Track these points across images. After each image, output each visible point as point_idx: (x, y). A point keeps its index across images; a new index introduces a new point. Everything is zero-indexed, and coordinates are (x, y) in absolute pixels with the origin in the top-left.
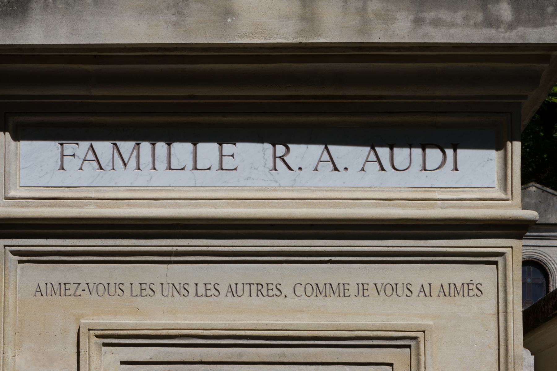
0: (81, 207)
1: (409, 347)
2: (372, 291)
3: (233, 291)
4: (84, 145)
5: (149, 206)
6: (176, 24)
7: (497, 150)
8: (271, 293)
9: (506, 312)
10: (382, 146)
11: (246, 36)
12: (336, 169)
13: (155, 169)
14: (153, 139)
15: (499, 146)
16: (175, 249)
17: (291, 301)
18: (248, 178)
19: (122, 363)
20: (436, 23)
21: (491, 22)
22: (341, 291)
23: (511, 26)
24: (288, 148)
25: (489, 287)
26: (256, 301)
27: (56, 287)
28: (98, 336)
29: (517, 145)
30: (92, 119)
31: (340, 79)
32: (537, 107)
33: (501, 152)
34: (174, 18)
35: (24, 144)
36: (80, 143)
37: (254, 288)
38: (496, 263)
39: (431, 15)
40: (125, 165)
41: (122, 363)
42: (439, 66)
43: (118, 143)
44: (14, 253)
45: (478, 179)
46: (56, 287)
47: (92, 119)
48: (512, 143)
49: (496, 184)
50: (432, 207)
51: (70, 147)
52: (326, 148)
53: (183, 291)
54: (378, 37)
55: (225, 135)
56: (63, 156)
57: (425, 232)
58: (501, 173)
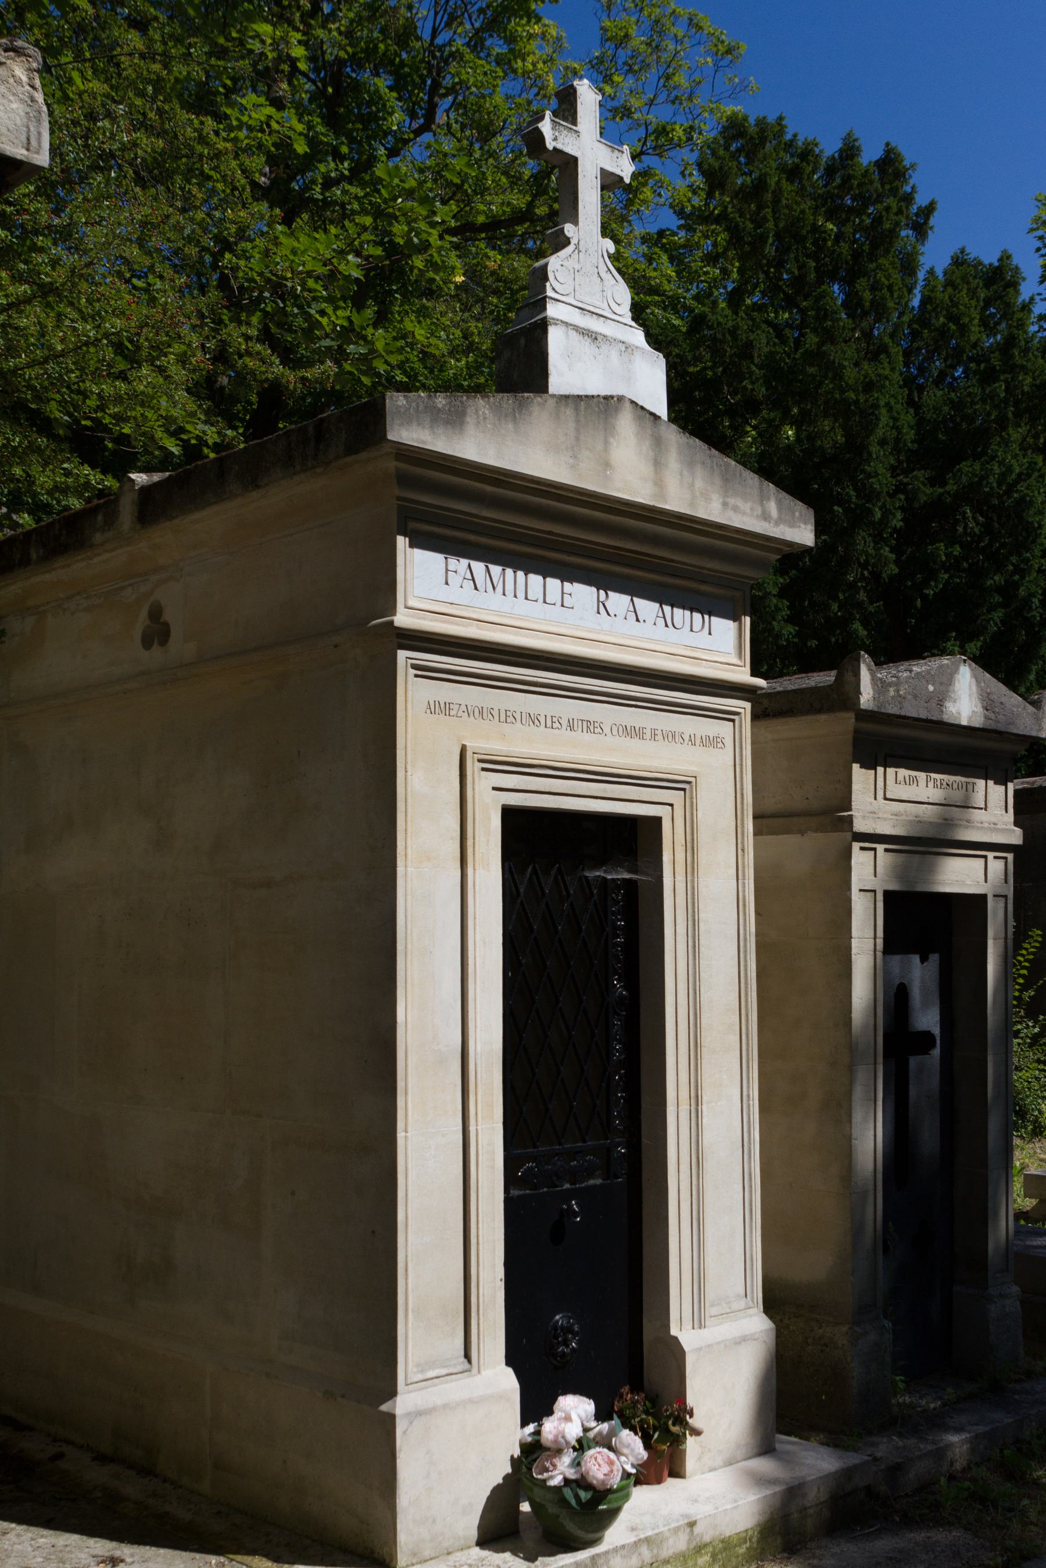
0: (495, 631)
1: (684, 790)
2: (659, 737)
3: (692, 741)
4: (464, 562)
5: (517, 634)
6: (572, 467)
7: (734, 621)
8: (555, 725)
9: (741, 765)
10: (666, 604)
11: (619, 491)
12: (638, 620)
13: (504, 594)
14: (516, 568)
15: (735, 618)
16: (535, 679)
17: (609, 739)
18: (581, 618)
19: (494, 789)
20: (736, 509)
21: (765, 517)
22: (553, 723)
23: (777, 524)
24: (607, 594)
25: (729, 741)
26: (588, 737)
27: (442, 706)
28: (480, 761)
29: (748, 619)
30: (472, 537)
31: (656, 540)
32: (255, 494)
33: (736, 624)
34: (571, 461)
35: (418, 552)
36: (461, 560)
37: (585, 723)
38: (733, 721)
39: (732, 501)
40: (494, 588)
41: (494, 789)
42: (718, 543)
43: (490, 566)
44: (415, 667)
45: (716, 646)
46: (442, 706)
47: (472, 537)
48: (607, 594)
49: (732, 651)
50: (699, 665)
51: (453, 562)
52: (632, 600)
53: (536, 722)
54: (701, 513)
55: (568, 574)
56: (447, 570)
57: (507, 658)
58: (737, 642)
